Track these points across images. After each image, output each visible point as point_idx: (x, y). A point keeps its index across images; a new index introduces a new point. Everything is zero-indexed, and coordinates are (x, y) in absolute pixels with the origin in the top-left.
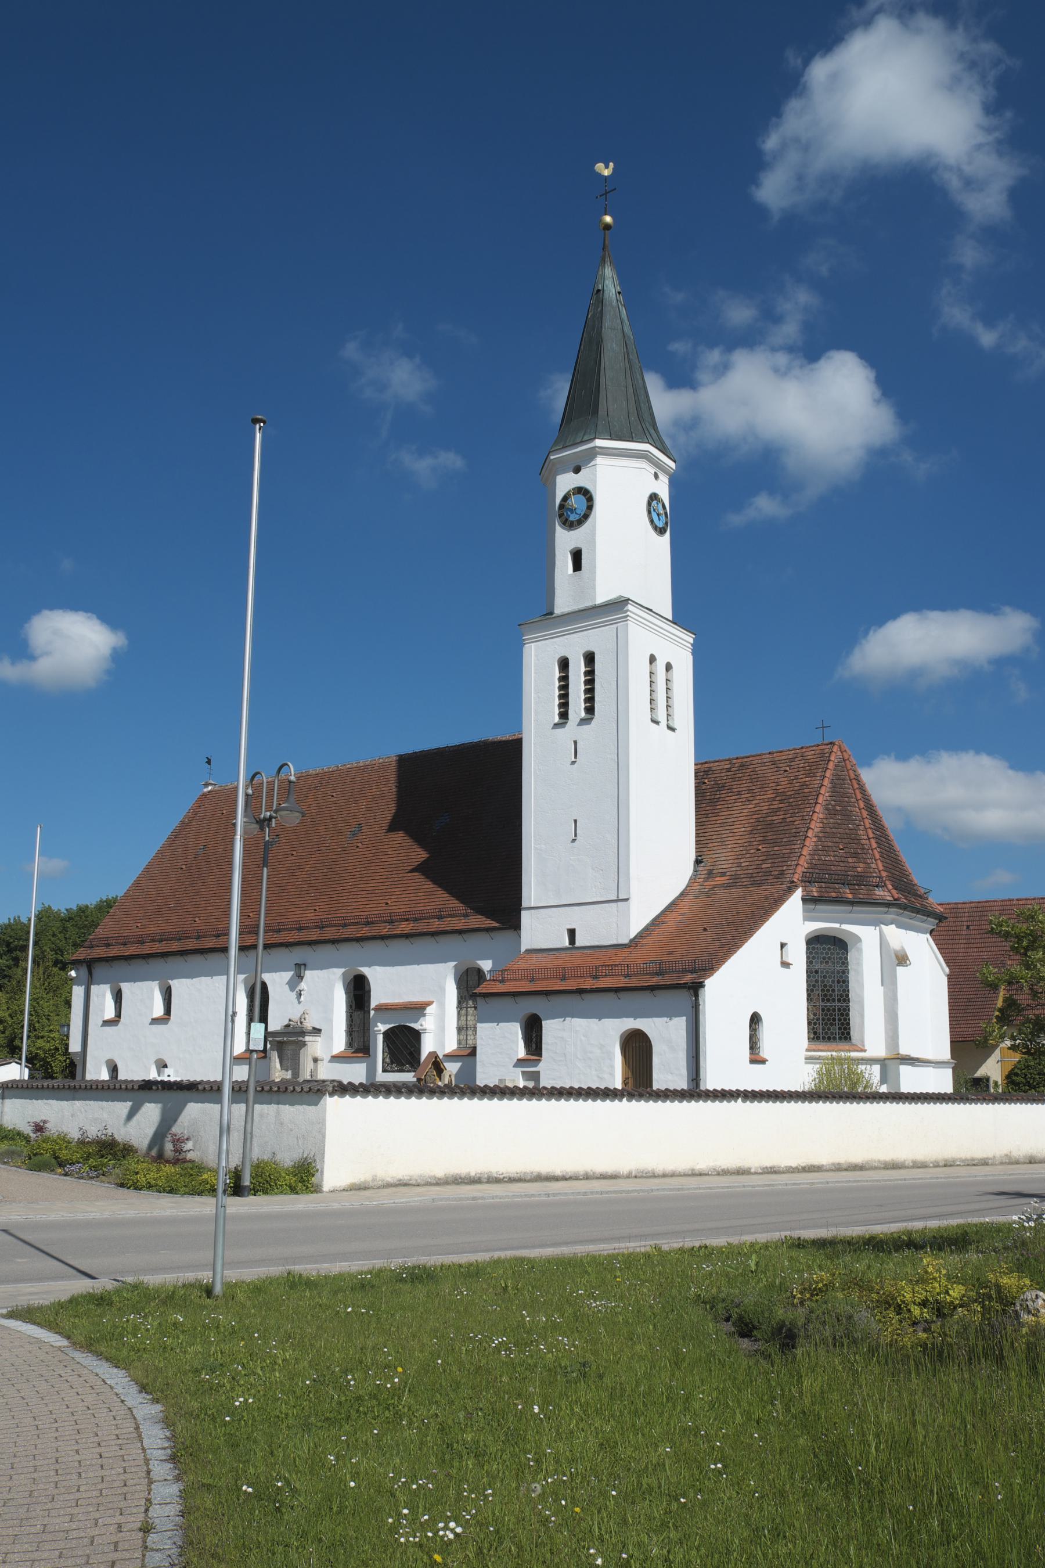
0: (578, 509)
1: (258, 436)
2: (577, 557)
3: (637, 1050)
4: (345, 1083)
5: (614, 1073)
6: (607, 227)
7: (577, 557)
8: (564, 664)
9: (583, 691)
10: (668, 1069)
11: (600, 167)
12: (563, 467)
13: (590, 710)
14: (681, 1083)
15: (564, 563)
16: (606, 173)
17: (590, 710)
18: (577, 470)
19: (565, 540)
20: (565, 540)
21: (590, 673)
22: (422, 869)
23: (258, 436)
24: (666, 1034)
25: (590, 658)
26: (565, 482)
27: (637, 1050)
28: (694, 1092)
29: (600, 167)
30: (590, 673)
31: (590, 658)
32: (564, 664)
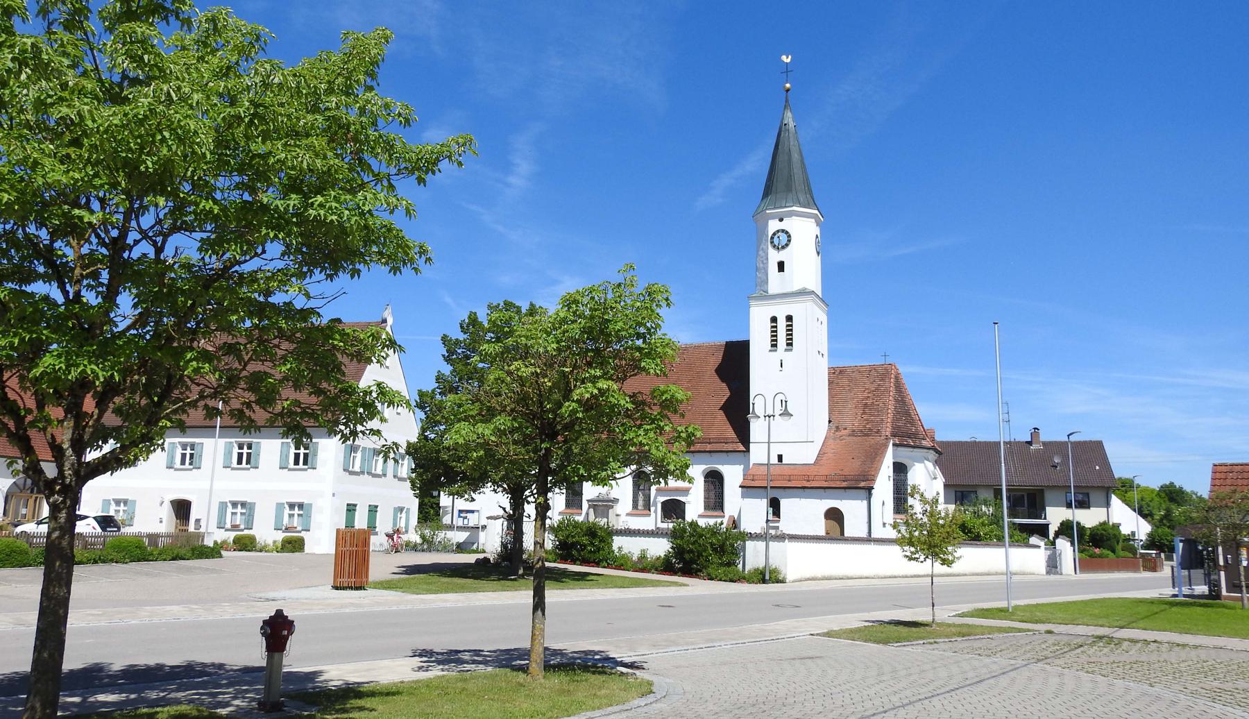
0: (783, 241)
1: (101, 698)
2: (781, 266)
3: (834, 516)
4: (1199, 485)
5: (820, 528)
6: (788, 90)
7: (781, 266)
8: (774, 320)
9: (784, 334)
10: (854, 526)
11: (784, 58)
12: (773, 217)
13: (790, 345)
14: (864, 534)
15: (773, 267)
16: (789, 60)
17: (790, 345)
18: (781, 220)
19: (774, 256)
20: (774, 256)
21: (790, 330)
22: (338, 531)
23: (101, 698)
24: (852, 509)
25: (789, 318)
26: (774, 226)
27: (834, 516)
28: (869, 540)
29: (784, 58)
30: (790, 330)
31: (789, 318)
32: (774, 320)
